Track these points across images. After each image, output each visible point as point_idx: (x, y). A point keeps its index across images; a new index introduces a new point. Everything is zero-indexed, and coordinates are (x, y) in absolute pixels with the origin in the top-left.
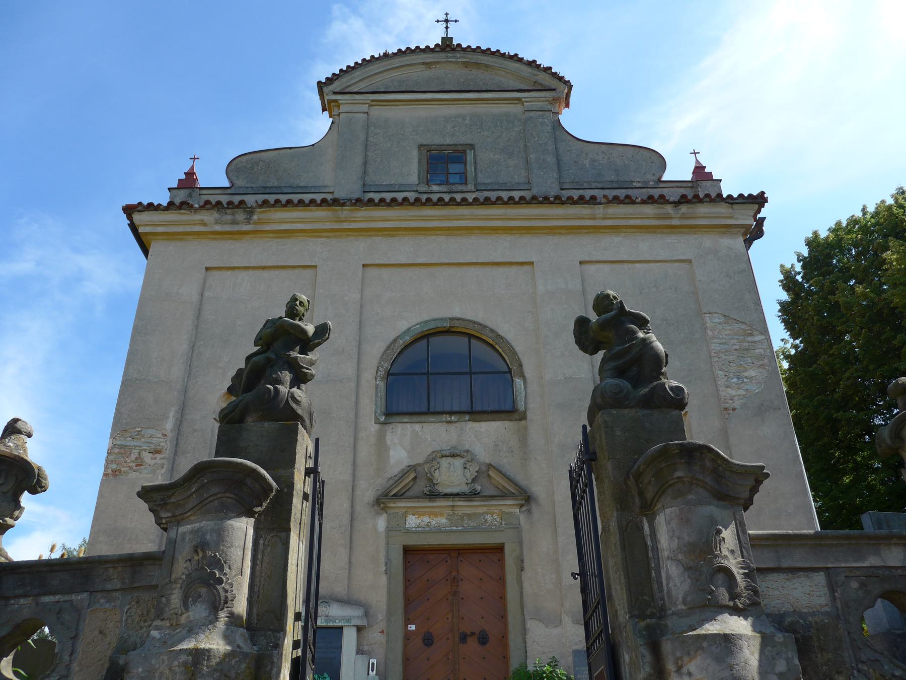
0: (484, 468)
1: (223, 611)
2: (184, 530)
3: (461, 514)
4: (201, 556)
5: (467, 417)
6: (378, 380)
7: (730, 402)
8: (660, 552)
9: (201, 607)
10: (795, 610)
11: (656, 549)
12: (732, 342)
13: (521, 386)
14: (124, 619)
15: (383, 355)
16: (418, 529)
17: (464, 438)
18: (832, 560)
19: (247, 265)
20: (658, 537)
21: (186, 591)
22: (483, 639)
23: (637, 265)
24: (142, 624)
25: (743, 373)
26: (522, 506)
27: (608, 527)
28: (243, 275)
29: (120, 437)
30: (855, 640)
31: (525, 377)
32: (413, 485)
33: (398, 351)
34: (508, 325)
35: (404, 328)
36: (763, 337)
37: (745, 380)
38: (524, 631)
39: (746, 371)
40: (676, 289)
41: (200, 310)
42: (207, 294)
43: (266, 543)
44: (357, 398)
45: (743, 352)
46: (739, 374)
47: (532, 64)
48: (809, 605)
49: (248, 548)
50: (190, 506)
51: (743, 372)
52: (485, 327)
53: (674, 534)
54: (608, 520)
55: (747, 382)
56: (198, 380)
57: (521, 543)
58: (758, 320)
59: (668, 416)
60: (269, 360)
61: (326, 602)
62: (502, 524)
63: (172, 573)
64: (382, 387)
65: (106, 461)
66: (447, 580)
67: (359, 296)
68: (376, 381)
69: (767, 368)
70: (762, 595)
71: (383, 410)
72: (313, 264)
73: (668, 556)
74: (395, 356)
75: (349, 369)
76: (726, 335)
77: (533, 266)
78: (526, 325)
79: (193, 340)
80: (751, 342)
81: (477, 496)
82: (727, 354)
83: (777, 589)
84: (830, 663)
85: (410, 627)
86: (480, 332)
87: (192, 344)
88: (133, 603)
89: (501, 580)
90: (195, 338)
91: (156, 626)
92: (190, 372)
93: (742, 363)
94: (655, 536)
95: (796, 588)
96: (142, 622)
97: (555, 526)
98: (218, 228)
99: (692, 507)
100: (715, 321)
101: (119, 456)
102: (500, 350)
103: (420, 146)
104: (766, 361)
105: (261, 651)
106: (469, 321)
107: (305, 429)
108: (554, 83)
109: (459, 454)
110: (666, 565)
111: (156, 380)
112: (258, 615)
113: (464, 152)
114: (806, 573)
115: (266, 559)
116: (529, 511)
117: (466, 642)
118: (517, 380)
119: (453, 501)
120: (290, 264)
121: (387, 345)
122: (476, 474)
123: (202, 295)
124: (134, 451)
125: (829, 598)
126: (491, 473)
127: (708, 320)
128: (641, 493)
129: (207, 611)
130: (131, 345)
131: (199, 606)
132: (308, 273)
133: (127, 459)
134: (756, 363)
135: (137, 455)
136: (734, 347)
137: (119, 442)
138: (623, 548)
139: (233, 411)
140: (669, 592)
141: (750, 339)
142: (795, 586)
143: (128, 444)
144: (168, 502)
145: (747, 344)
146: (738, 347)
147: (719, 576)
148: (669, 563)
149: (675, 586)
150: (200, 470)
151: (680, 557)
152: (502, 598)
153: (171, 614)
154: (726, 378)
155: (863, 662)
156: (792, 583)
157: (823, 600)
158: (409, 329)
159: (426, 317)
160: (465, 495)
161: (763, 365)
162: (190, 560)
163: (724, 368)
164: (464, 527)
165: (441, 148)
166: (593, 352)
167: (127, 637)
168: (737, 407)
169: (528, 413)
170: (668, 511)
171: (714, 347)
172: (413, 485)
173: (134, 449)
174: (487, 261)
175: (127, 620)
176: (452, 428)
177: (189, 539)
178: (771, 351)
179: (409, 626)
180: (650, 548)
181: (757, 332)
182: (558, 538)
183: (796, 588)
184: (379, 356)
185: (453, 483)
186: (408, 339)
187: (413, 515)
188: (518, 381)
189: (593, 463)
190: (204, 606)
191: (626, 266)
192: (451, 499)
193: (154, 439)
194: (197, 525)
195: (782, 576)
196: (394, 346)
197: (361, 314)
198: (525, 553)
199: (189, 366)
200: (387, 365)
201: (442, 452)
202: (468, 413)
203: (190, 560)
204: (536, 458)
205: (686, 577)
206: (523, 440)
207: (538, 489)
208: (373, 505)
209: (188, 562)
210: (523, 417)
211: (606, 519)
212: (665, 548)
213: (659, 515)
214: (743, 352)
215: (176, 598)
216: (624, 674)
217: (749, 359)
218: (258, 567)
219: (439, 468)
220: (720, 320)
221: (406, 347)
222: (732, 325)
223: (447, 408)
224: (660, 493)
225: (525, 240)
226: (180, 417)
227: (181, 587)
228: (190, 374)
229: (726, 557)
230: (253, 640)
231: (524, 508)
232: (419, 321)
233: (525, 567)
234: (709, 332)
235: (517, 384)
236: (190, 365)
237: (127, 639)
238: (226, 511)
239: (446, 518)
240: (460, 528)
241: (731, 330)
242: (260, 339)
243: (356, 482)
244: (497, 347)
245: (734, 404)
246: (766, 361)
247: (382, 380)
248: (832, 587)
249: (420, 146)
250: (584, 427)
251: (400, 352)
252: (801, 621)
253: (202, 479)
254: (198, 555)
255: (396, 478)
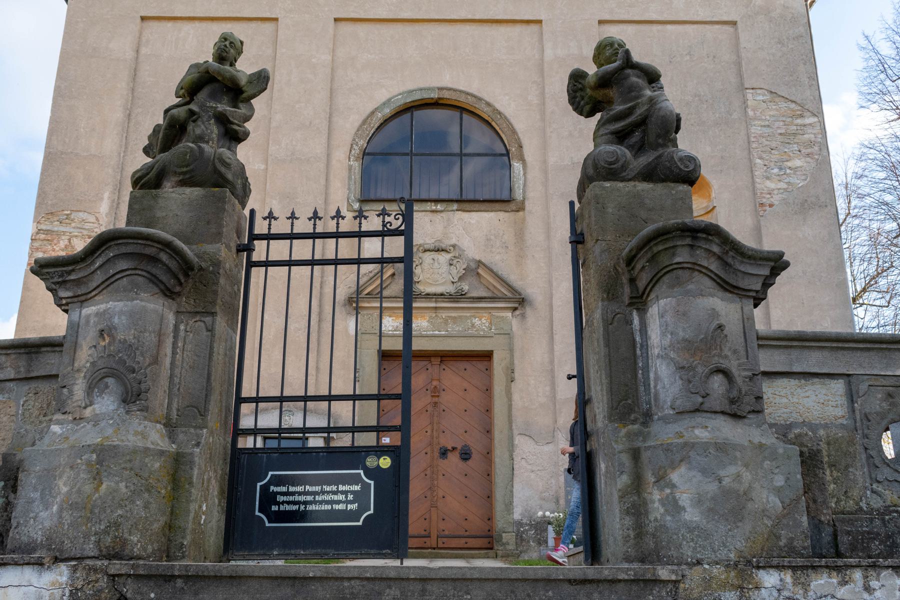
0: (473, 265)
1: (135, 404)
2: (88, 312)
3: (446, 317)
4: (107, 341)
5: (455, 206)
6: (351, 160)
7: (768, 196)
8: (649, 349)
9: (108, 400)
10: (804, 421)
11: (645, 346)
12: (777, 124)
13: (520, 171)
14: (20, 412)
15: (358, 130)
16: (395, 333)
17: (450, 231)
18: (855, 366)
19: (192, 15)
20: (649, 333)
21: (90, 381)
22: (466, 455)
23: (669, 27)
24: (41, 418)
25: (786, 163)
26: (515, 309)
27: (592, 321)
28: (187, 27)
29: (45, 221)
30: (873, 457)
31: (525, 160)
32: (391, 283)
33: (376, 126)
34: (507, 98)
35: (384, 99)
36: (816, 119)
37: (788, 171)
38: (511, 447)
39: (790, 160)
40: (714, 57)
41: (135, 70)
42: (143, 51)
43: (188, 329)
44: (327, 180)
45: (788, 137)
46: (781, 164)
48: (821, 416)
50: (95, 284)
51: (787, 161)
52: (480, 99)
53: (666, 329)
54: (592, 312)
55: (790, 173)
56: (137, 155)
57: (511, 351)
58: (812, 98)
59: (674, 192)
60: (192, 113)
61: (290, 411)
62: (491, 329)
63: (75, 362)
64: (357, 168)
65: (31, 248)
66: (427, 390)
67: (330, 58)
68: (349, 160)
69: (816, 157)
70: (766, 403)
71: (358, 196)
72: (273, 16)
73: (659, 354)
74: (372, 132)
75: (318, 147)
76: (770, 116)
77: (542, 26)
78: (529, 99)
79: (129, 107)
80: (800, 125)
81: (463, 297)
82: (768, 139)
83: (786, 397)
84: (839, 482)
85: (385, 440)
86: (474, 105)
87: (128, 112)
88: (30, 395)
89: (488, 391)
90: (132, 104)
91: (56, 420)
93: (786, 150)
94: (646, 332)
95: (808, 397)
96: (42, 416)
97: (552, 333)
99: (691, 298)
100: (758, 98)
101: (45, 242)
102: (497, 128)
104: (816, 148)
105: (181, 449)
106: (461, 91)
107: (236, 197)
109: (444, 248)
110: (656, 364)
111: (85, 154)
112: (178, 410)
114: (822, 380)
115: (189, 347)
116: (523, 316)
117: (446, 458)
118: (515, 164)
119: (436, 302)
120: (245, 16)
121: (363, 118)
122: (464, 272)
123: (137, 51)
124: (63, 237)
125: (846, 410)
126: (480, 271)
127: (749, 96)
128: (632, 281)
129: (116, 404)
130: (52, 111)
131: (106, 399)
132: (268, 27)
133: (55, 247)
134: (803, 151)
135: (66, 242)
136: (779, 131)
137: (43, 227)
138: (607, 345)
139: (148, 174)
140: (656, 395)
141: (799, 121)
142: (807, 394)
143: (56, 229)
144: (67, 279)
145: (795, 128)
146: (783, 131)
147: (715, 378)
148: (658, 362)
149: (664, 388)
150: (103, 242)
151: (672, 354)
152: (489, 410)
153: (74, 407)
154: (765, 168)
155: (879, 482)
156: (804, 390)
157: (840, 412)
158: (389, 100)
159: (410, 86)
160: (450, 295)
161: (812, 154)
162: (95, 347)
163: (764, 156)
164: (447, 331)
165: (784, 275)
166: (590, 114)
167: (24, 432)
168: (776, 203)
169: (527, 203)
170: (662, 302)
171: (756, 130)
172: (391, 283)
173: (64, 235)
174: (486, 18)
175: (23, 414)
176: (437, 218)
177: (94, 322)
178: (823, 137)
179: (383, 439)
180: (638, 345)
181: (808, 113)
182: (555, 347)
183: (808, 397)
184: (353, 131)
185: (437, 281)
186: (387, 111)
187: (390, 317)
188: (517, 165)
189: (580, 246)
190: (112, 399)
191: (655, 28)
192: (434, 300)
193: (86, 224)
194: (103, 307)
195: (793, 382)
196: (372, 120)
197: (332, 80)
198: (516, 362)
199: (124, 138)
200: (362, 143)
201: (425, 246)
202: (457, 201)
203: (95, 347)
204: (533, 256)
205: (677, 378)
206: (520, 234)
207: (533, 288)
208: (345, 305)
209: (93, 349)
210: (521, 208)
211: (591, 311)
212: (655, 345)
213: (652, 307)
214: (788, 137)
215: (79, 389)
216: (599, 485)
217: (795, 146)
218: (178, 356)
219: (421, 264)
220: (765, 98)
221: (386, 121)
222: (779, 103)
223: (434, 196)
224: (654, 281)
226: (117, 198)
227: (85, 377)
228: (126, 148)
229: (726, 357)
230: (172, 437)
231: (517, 312)
232: (401, 91)
233: (516, 378)
234: (749, 112)
235: (516, 169)
236: (126, 137)
237: (24, 434)
238: (138, 290)
239: (428, 321)
240: (443, 333)
241: (777, 110)
242: (182, 88)
243: (325, 278)
244: (493, 124)
245: (772, 200)
246: (816, 148)
247: (356, 160)
248: (851, 397)
250: (572, 204)
251: (379, 127)
252: (810, 433)
253: (107, 252)
254: (104, 339)
255: (371, 275)
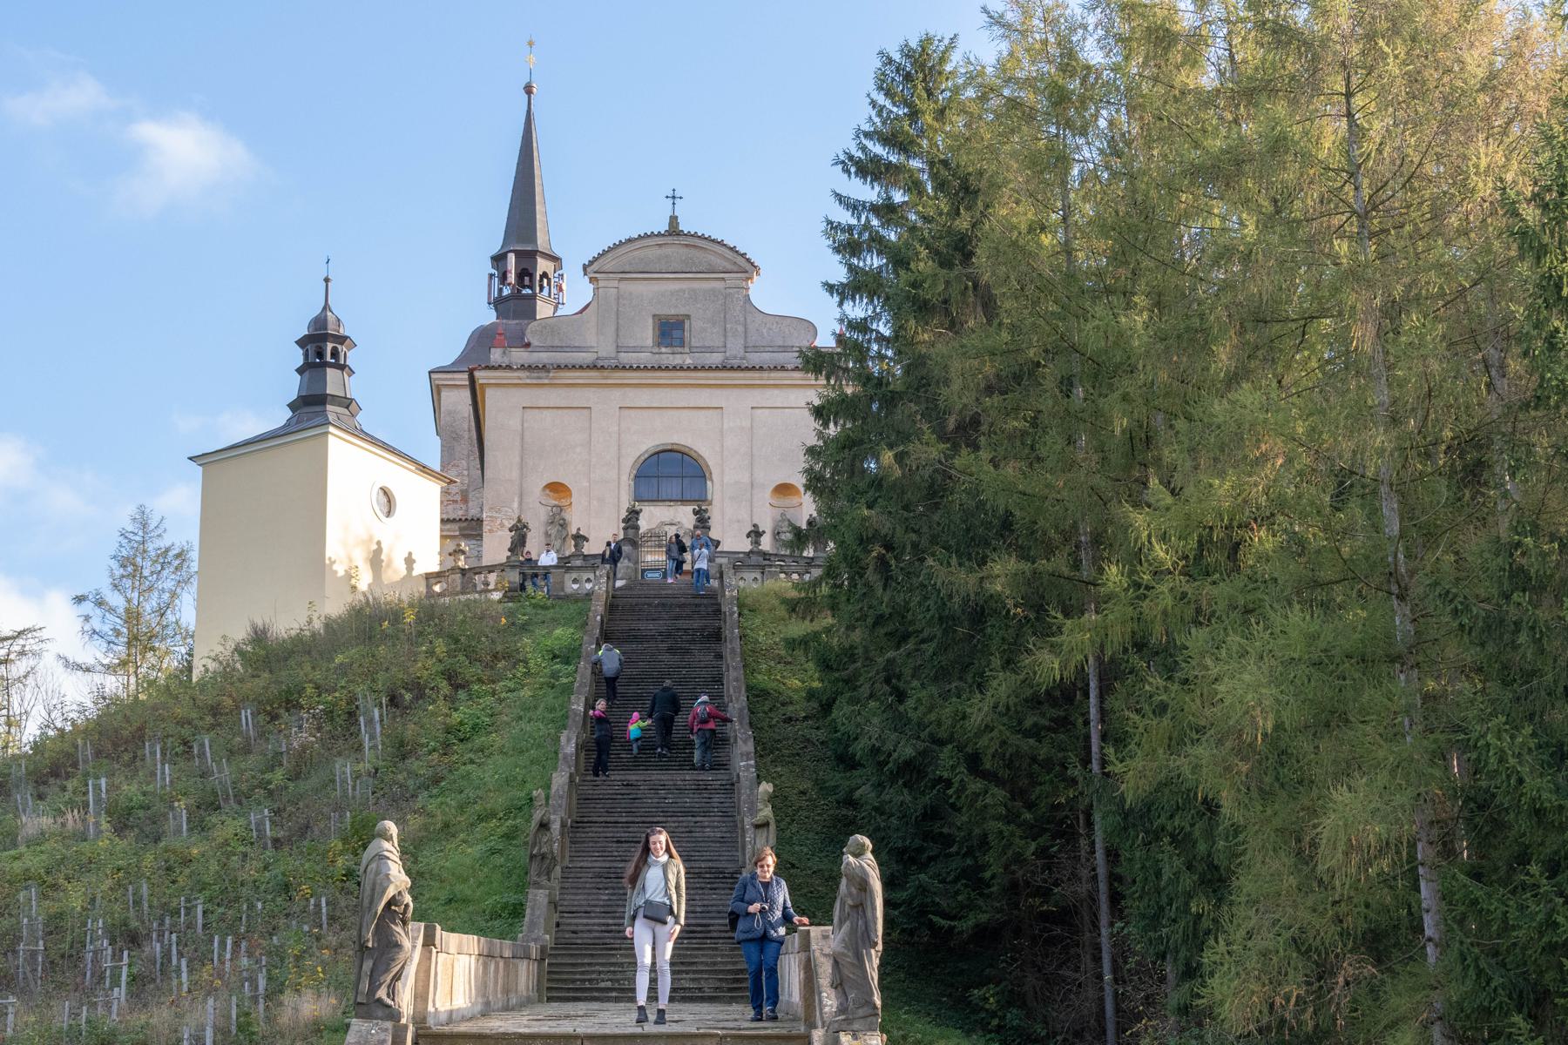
28: (545, 412)
47: (733, 249)
49: (663, 971)
92: (522, 476)
98: (528, 381)
103: (654, 316)
108: (748, 266)
113: (683, 322)
132: (586, 412)
159: (658, 443)
188: (709, 483)
225: (718, 392)
249: (654, 316)
